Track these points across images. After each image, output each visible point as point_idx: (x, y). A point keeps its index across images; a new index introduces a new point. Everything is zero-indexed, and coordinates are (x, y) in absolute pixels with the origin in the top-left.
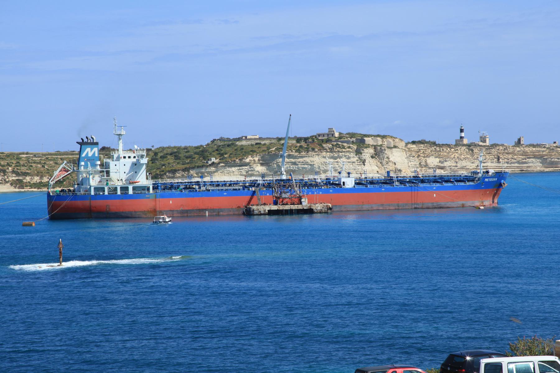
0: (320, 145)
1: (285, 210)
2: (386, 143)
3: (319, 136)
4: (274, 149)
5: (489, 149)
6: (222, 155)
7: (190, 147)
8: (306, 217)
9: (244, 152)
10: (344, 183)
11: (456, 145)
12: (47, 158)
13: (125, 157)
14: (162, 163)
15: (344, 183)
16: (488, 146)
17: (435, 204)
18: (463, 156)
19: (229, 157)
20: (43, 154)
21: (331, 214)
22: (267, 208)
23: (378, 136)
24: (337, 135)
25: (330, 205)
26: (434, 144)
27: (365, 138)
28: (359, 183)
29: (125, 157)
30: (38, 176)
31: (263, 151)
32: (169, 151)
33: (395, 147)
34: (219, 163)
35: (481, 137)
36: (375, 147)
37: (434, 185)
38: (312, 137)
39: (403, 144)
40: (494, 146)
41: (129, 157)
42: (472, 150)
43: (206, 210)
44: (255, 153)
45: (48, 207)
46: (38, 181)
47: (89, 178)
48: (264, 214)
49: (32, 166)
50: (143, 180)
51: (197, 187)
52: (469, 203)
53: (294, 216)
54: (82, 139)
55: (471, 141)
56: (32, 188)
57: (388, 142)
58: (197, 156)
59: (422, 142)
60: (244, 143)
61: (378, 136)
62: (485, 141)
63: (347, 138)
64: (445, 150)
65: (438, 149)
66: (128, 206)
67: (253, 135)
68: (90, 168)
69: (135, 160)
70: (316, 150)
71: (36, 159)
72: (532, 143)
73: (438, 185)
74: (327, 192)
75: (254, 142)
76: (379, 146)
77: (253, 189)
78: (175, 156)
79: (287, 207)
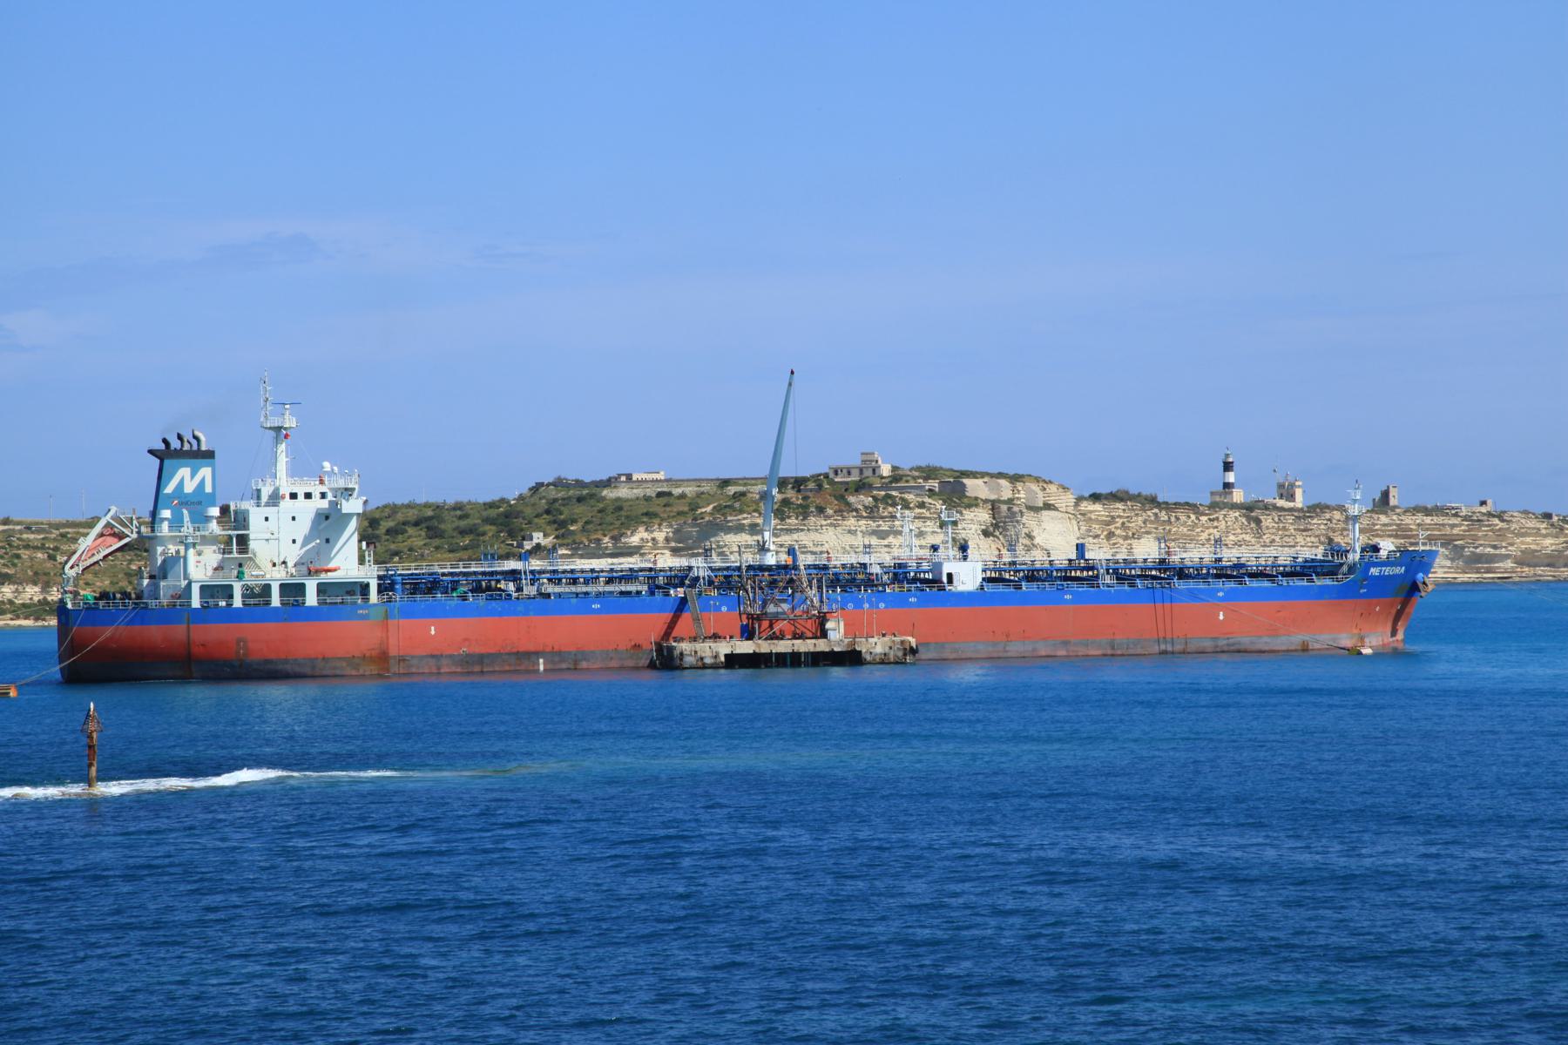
0: (841, 498)
1: (778, 655)
2: (1022, 495)
3: (836, 473)
4: (709, 509)
5: (1305, 517)
6: (562, 524)
7: (469, 503)
8: (838, 673)
9: (625, 516)
10: (950, 576)
11: (1214, 506)
12: (63, 535)
13: (294, 496)
14: (393, 547)
15: (950, 576)
16: (1301, 510)
17: (1222, 643)
18: (1232, 537)
19: (584, 530)
20: (50, 525)
21: (913, 664)
22: (724, 649)
23: (1001, 475)
24: (886, 470)
25: (913, 641)
26: (1152, 501)
27: (965, 481)
28: (994, 579)
29: (294, 496)
30: (35, 584)
31: (680, 513)
32: (412, 515)
33: (1048, 506)
34: (554, 548)
35: (1281, 486)
36: (994, 506)
37: (1220, 584)
38: (816, 478)
39: (1070, 499)
40: (1316, 509)
41: (308, 496)
42: (1258, 521)
43: (538, 654)
44: (657, 521)
45: (60, 643)
46: (36, 599)
47: (185, 558)
48: (715, 667)
49: (18, 556)
50: (348, 562)
51: (511, 587)
52: (1321, 639)
53: (803, 669)
54: (165, 441)
55: (1254, 497)
56: (18, 618)
57: (1029, 491)
58: (490, 530)
59: (1115, 497)
60: (623, 492)
61: (1001, 475)
62: (1292, 497)
63: (915, 478)
64: (1183, 518)
65: (1163, 516)
66: (304, 640)
67: (650, 473)
68: (188, 528)
69: (324, 504)
70: (830, 512)
71: (32, 536)
72: (1421, 503)
73: (1231, 585)
74: (901, 601)
75: (651, 492)
76: (1004, 502)
77: (681, 592)
78: (428, 528)
79: (783, 646)
